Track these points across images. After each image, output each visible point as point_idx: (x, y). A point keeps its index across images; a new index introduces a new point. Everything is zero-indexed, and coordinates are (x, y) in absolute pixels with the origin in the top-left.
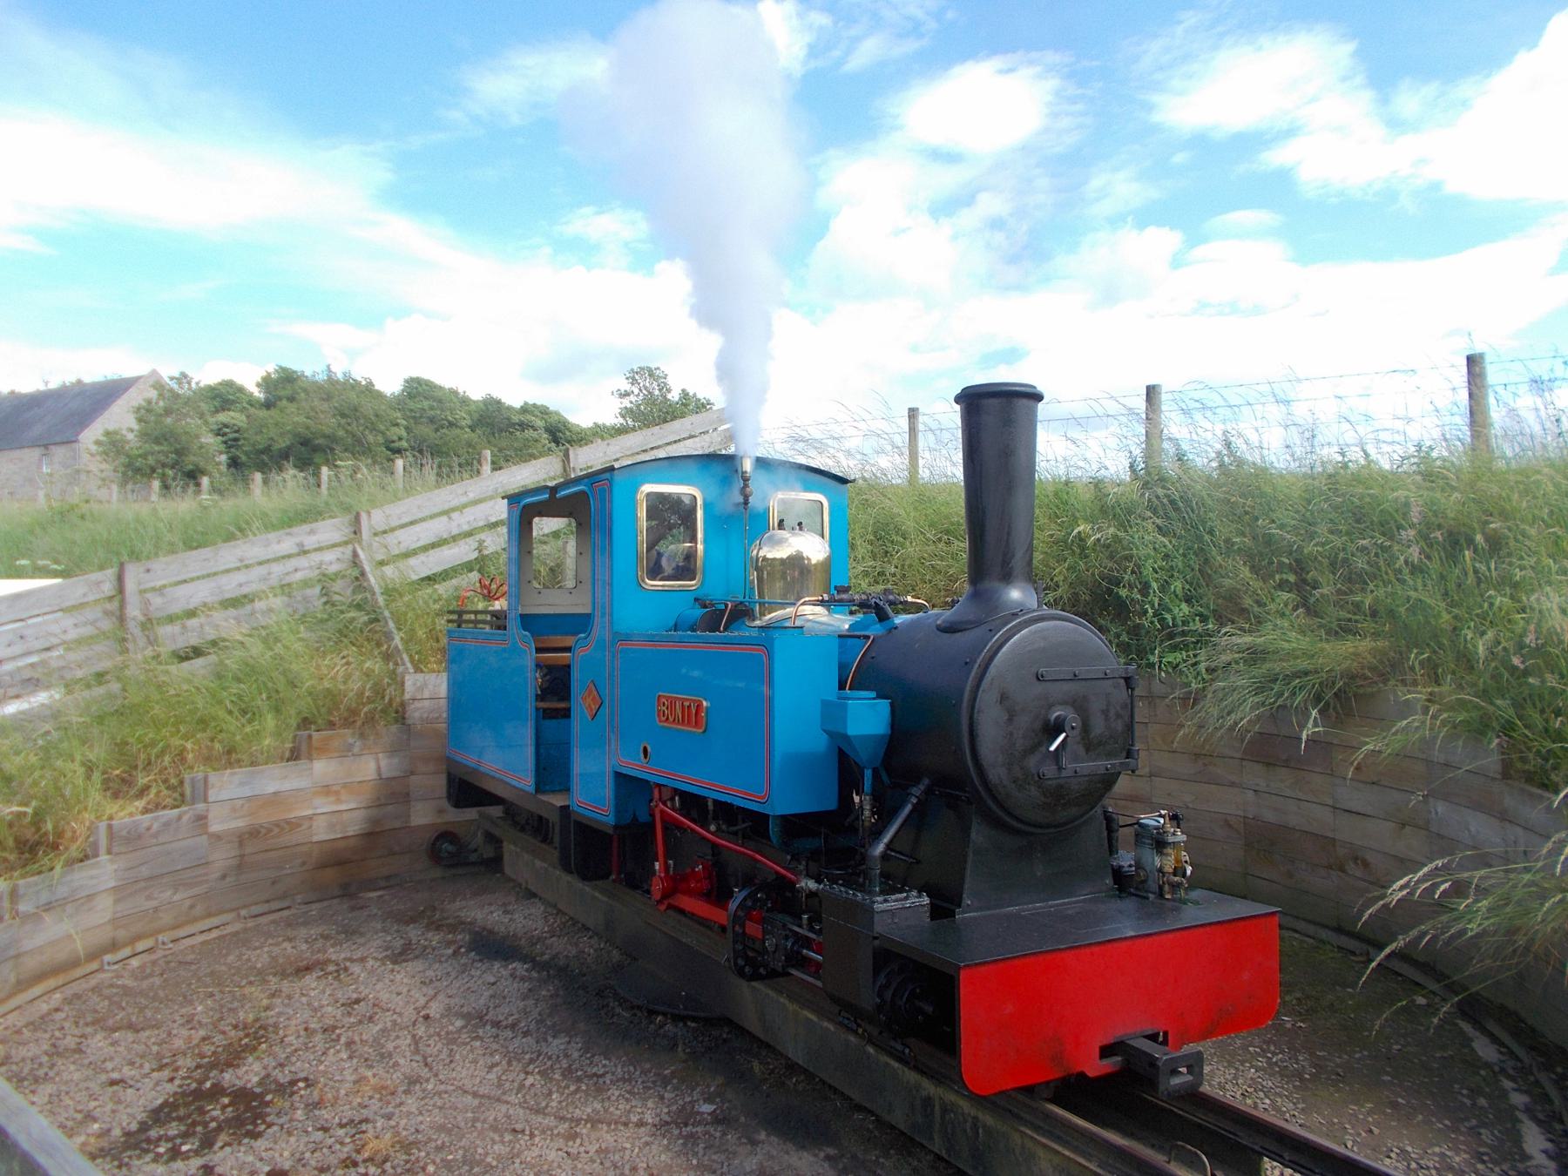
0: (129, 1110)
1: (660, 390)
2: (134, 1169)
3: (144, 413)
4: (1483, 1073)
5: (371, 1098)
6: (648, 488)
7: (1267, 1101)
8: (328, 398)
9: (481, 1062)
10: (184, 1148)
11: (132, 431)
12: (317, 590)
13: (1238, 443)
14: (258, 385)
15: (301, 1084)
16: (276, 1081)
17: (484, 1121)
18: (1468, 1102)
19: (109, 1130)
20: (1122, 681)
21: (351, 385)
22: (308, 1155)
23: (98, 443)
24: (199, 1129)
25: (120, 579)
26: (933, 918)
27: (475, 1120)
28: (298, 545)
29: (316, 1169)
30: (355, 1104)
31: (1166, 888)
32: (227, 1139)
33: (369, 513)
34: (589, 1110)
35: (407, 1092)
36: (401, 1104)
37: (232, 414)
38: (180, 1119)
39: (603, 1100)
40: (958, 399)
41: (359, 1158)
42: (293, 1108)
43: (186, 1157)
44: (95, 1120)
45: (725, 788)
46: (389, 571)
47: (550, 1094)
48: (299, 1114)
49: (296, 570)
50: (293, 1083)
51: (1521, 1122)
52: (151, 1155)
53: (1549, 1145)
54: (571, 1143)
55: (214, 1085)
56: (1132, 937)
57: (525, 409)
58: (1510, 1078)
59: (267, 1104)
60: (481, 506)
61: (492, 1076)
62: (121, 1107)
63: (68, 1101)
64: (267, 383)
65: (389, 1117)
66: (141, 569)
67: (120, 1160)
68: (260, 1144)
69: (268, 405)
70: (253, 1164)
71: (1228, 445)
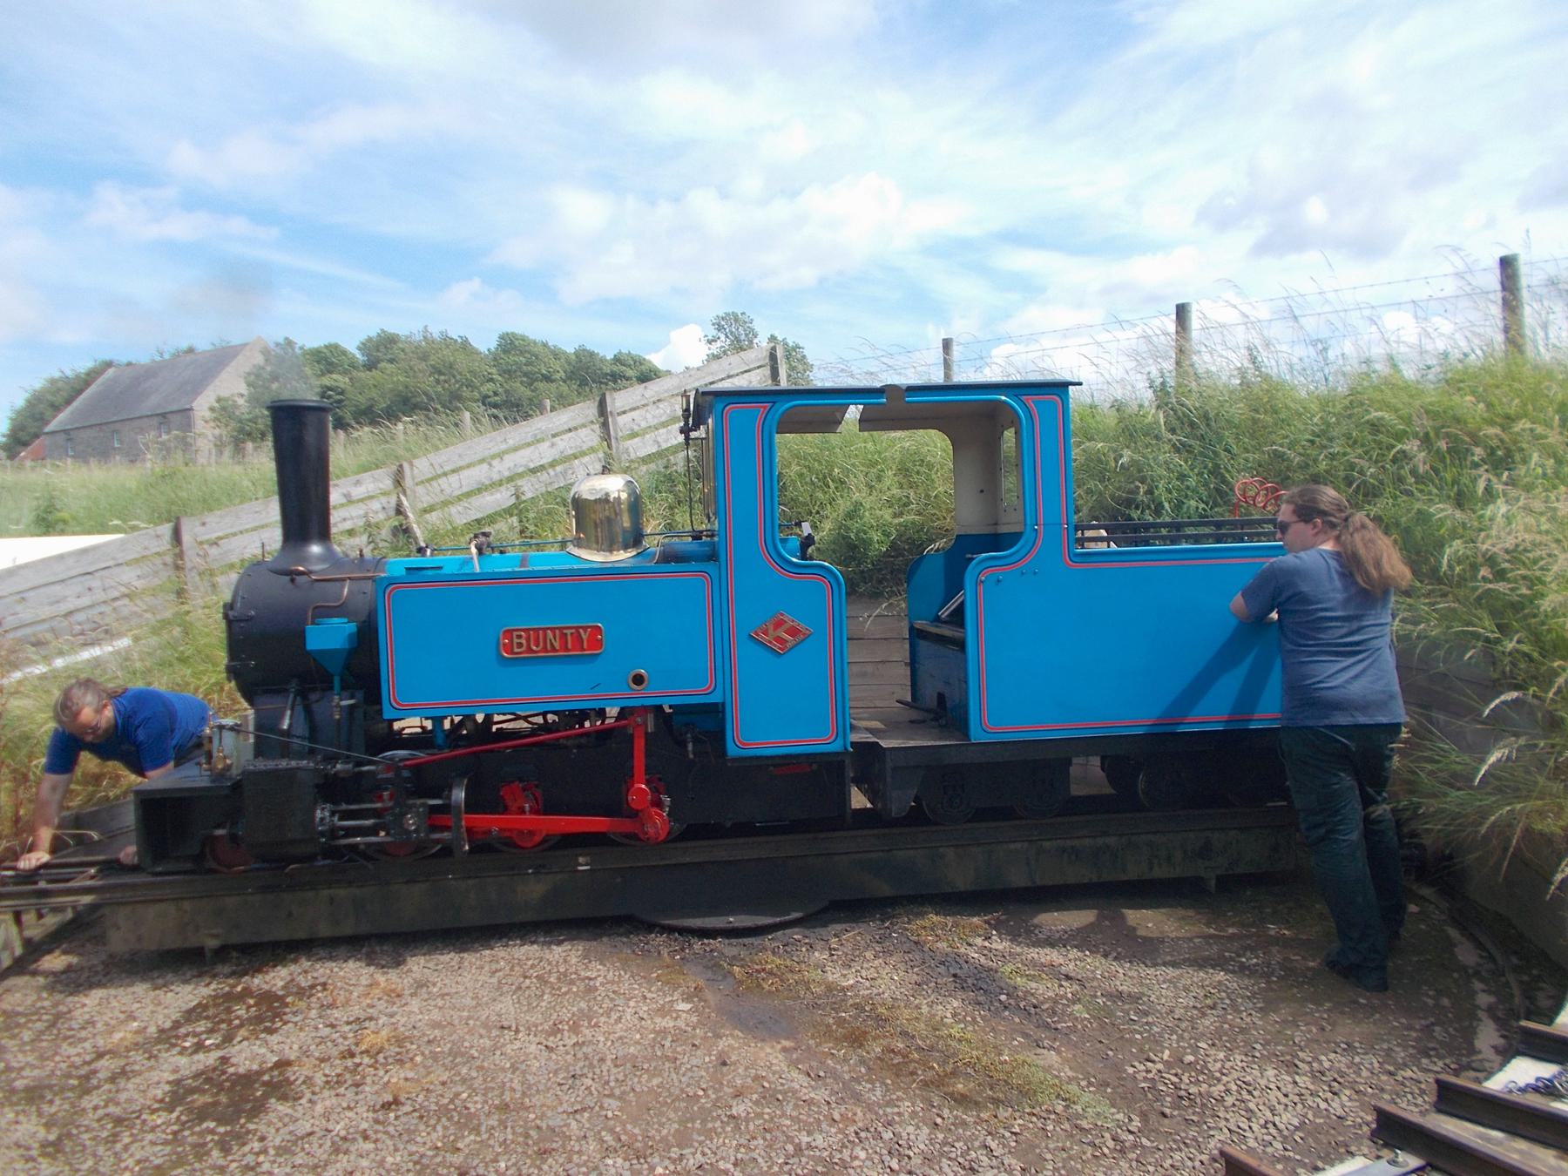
0: (166, 1011)
1: (746, 335)
2: (161, 1061)
3: (255, 379)
4: (1456, 975)
5: (379, 999)
7: (1228, 1001)
8: (424, 357)
9: (487, 968)
10: (208, 1042)
11: (242, 395)
12: (364, 538)
13: (1264, 357)
14: (359, 349)
15: (319, 988)
16: (298, 986)
17: (478, 1019)
18: (1431, 1002)
19: (145, 1028)
21: (447, 341)
22: (313, 1047)
23: (212, 409)
24: (224, 1026)
25: (177, 535)
27: (469, 1018)
28: (345, 495)
29: (317, 1059)
30: (364, 1004)
32: (246, 1034)
33: (411, 465)
34: (575, 1009)
35: (412, 995)
36: (406, 1004)
37: (334, 376)
38: (207, 1018)
39: (589, 1001)
41: (357, 1050)
42: (309, 1008)
43: (208, 1049)
44: (135, 1019)
46: (433, 517)
47: (543, 993)
48: (313, 1013)
49: (345, 520)
50: (313, 987)
51: (1480, 1020)
52: (178, 1049)
53: (1501, 1041)
54: (551, 1038)
55: (244, 989)
57: (617, 360)
58: (1482, 980)
59: (287, 1005)
60: (522, 452)
61: (494, 980)
62: (159, 1009)
63: (115, 1004)
64: (366, 346)
65: (392, 1016)
66: (197, 523)
67: (150, 1052)
68: (274, 1039)
69: (371, 365)
70: (264, 1056)
71: (1253, 360)
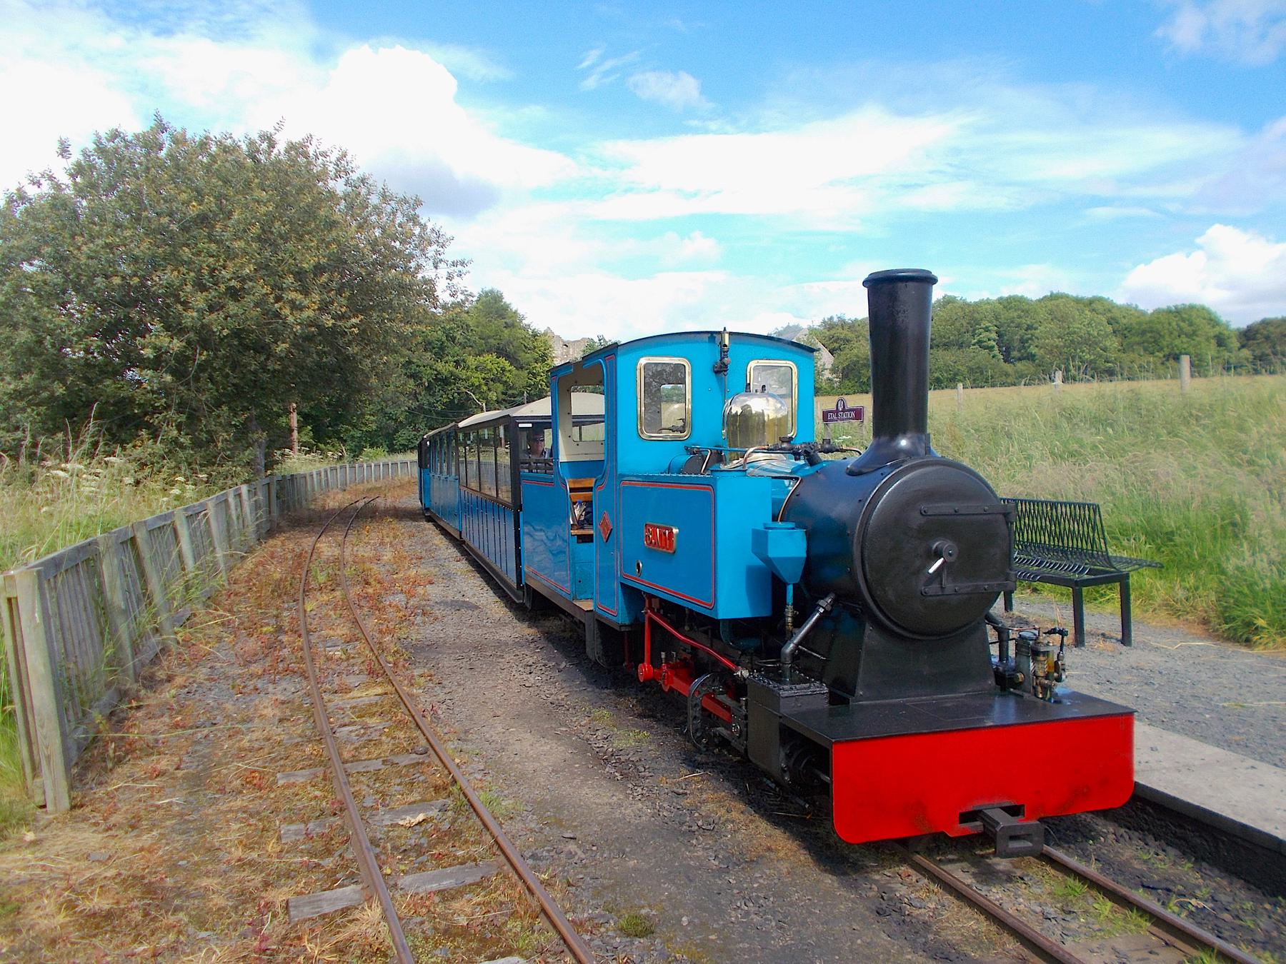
6: (643, 361)
20: (1001, 516)
26: (831, 703)
31: (1039, 689)
40: (864, 283)
45: (701, 602)
56: (990, 727)
